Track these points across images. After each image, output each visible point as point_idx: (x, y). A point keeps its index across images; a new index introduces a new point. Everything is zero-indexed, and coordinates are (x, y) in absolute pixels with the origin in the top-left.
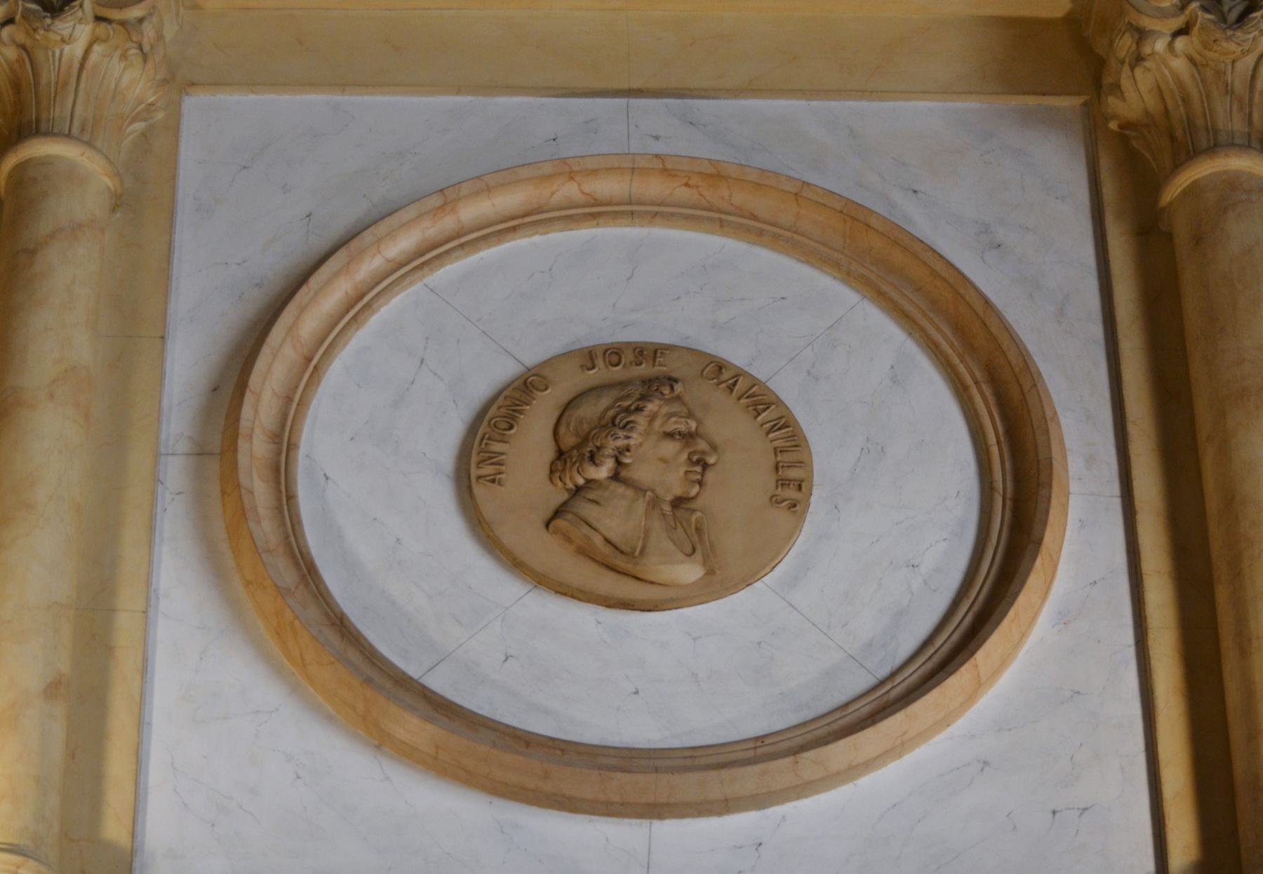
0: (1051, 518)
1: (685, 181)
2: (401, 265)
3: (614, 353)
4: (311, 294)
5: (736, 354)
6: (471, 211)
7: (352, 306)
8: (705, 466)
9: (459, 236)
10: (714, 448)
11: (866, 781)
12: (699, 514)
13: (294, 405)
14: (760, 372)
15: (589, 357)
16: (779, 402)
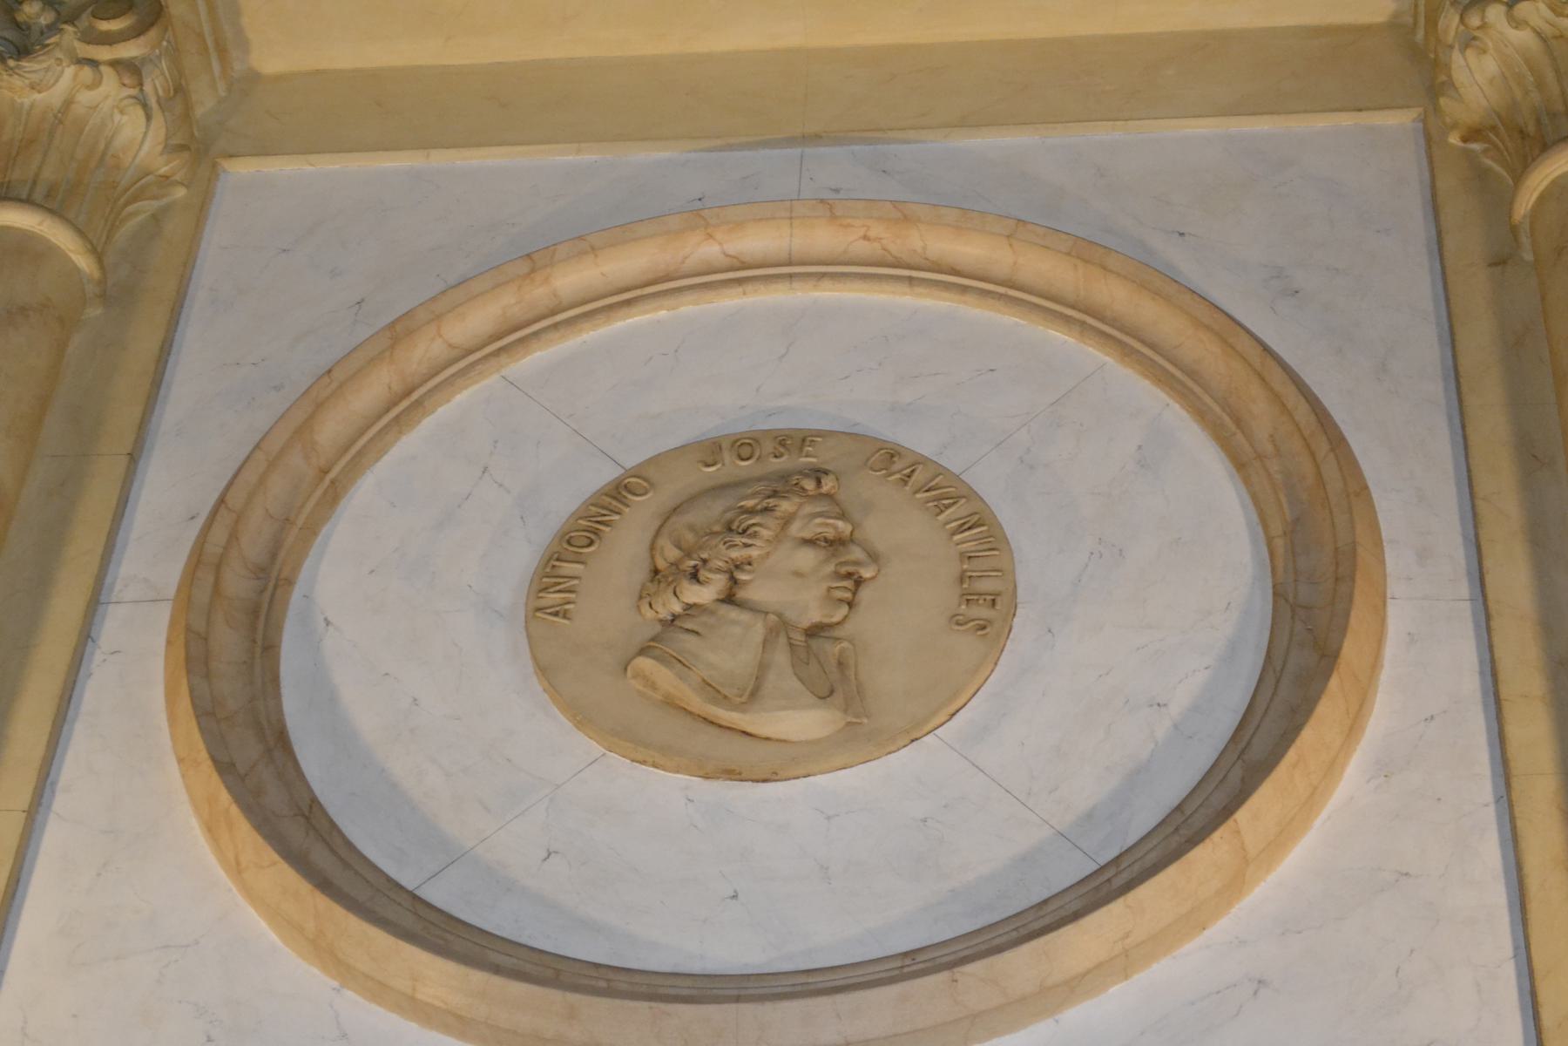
0: (1353, 621)
1: (862, 232)
2: (470, 352)
3: (745, 445)
4: (334, 385)
5: (920, 440)
6: (572, 279)
7: (395, 404)
8: (859, 582)
9: (553, 313)
10: (874, 557)
11: (1075, 1016)
12: (845, 644)
14: (953, 462)
15: (711, 450)
16: (971, 495)
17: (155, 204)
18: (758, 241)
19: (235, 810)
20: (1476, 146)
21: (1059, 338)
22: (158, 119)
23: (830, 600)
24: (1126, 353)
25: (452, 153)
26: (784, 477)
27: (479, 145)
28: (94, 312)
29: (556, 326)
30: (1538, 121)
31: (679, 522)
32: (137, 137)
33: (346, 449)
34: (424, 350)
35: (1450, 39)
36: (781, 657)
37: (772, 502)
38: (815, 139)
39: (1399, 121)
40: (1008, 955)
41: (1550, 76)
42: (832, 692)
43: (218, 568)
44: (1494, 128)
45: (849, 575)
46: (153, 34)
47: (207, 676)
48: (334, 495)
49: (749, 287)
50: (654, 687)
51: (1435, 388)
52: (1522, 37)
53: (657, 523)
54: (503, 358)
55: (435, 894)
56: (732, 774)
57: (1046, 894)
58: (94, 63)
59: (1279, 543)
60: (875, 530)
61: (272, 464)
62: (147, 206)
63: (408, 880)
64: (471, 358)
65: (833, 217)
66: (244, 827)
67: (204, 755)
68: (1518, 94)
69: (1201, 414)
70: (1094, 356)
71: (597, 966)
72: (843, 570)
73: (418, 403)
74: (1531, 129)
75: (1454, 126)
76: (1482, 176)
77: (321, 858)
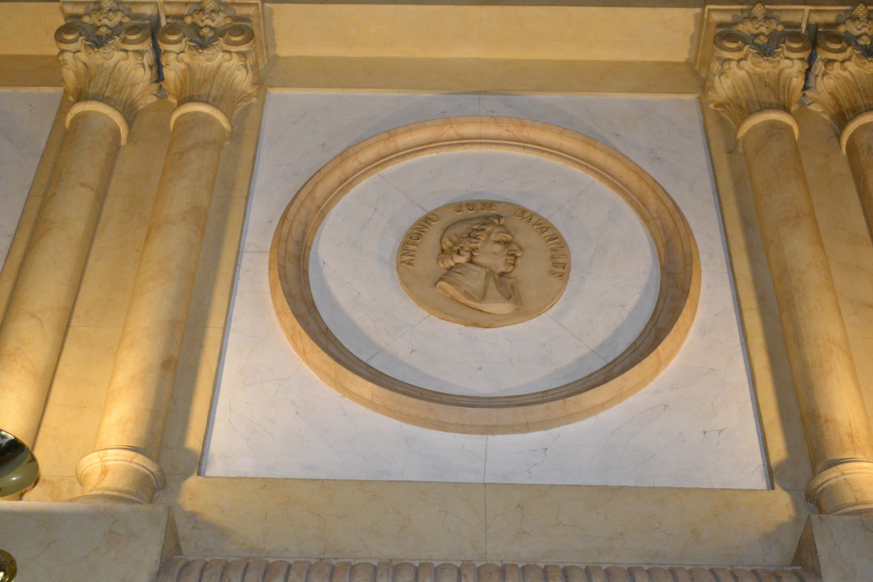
0: (693, 281)
3: (471, 205)
5: (532, 206)
6: (404, 140)
8: (516, 257)
10: (521, 249)
11: (603, 415)
14: (544, 214)
15: (459, 206)
16: (552, 227)
17: (246, 104)
18: (470, 130)
19: (302, 331)
20: (718, 109)
21: (578, 171)
22: (250, 74)
23: (506, 263)
24: (602, 178)
25: (353, 90)
26: (487, 217)
27: (364, 88)
28: (227, 143)
29: (398, 157)
30: (747, 104)
31: (450, 232)
32: (242, 79)
33: (326, 199)
34: (351, 164)
35: (715, 71)
36: (492, 284)
37: (484, 227)
38: (485, 92)
39: (691, 98)
40: (583, 394)
41: (751, 87)
42: (510, 297)
43: (286, 241)
44: (728, 104)
45: (513, 255)
46: (251, 42)
47: (287, 282)
48: (322, 216)
49: (466, 146)
50: (446, 292)
51: (710, 196)
52: (742, 73)
53: (441, 233)
54: (379, 168)
55: (373, 364)
56: (475, 325)
57: (590, 373)
58: (126, 51)
59: (662, 250)
60: (520, 238)
61: (302, 204)
62: (243, 104)
63: (363, 358)
64: (369, 167)
65: (496, 123)
66: (306, 338)
67: (289, 311)
68: (739, 92)
69: (631, 202)
70: (590, 178)
71: (435, 392)
72: (511, 253)
73: (350, 183)
74: (744, 106)
75: (712, 102)
76: (721, 120)
77: (331, 348)
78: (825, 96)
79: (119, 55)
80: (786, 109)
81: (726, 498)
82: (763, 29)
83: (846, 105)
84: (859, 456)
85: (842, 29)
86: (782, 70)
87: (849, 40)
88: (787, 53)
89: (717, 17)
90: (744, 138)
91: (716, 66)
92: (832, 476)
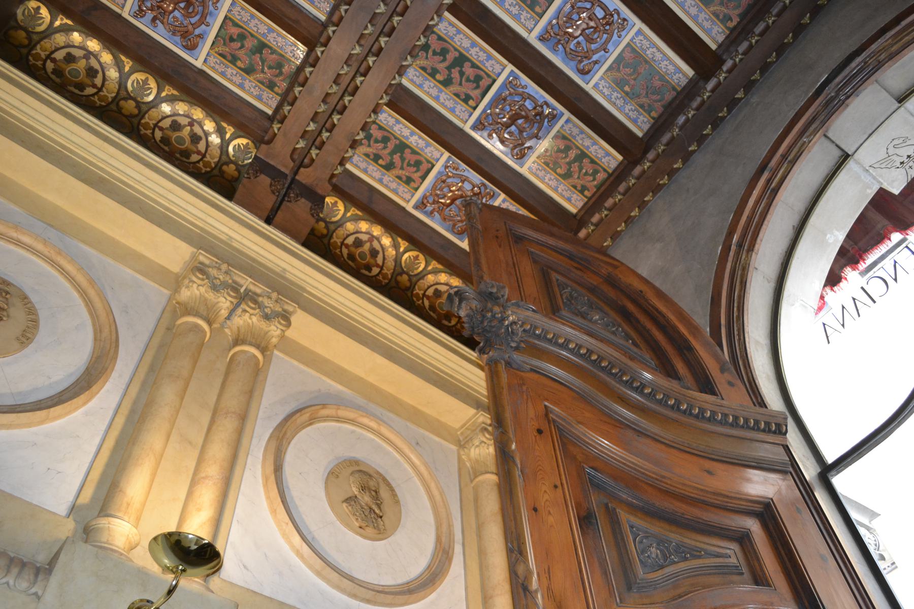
5: (34, 298)
10: (8, 316)
11: (16, 432)
13: (790, 568)
16: (37, 315)
18: (26, 239)
24: (87, 305)
38: (52, 226)
39: (167, 292)
52: (197, 292)
65: (45, 244)
69: (94, 325)
76: (175, 311)
78: (235, 328)
79: (273, 327)
80: (210, 323)
81: (34, 511)
82: (221, 277)
83: (241, 337)
84: (126, 518)
85: (260, 299)
86: (218, 303)
87: (260, 306)
88: (276, 323)
89: (201, 258)
90: (180, 325)
91: (186, 281)
92: (103, 522)
